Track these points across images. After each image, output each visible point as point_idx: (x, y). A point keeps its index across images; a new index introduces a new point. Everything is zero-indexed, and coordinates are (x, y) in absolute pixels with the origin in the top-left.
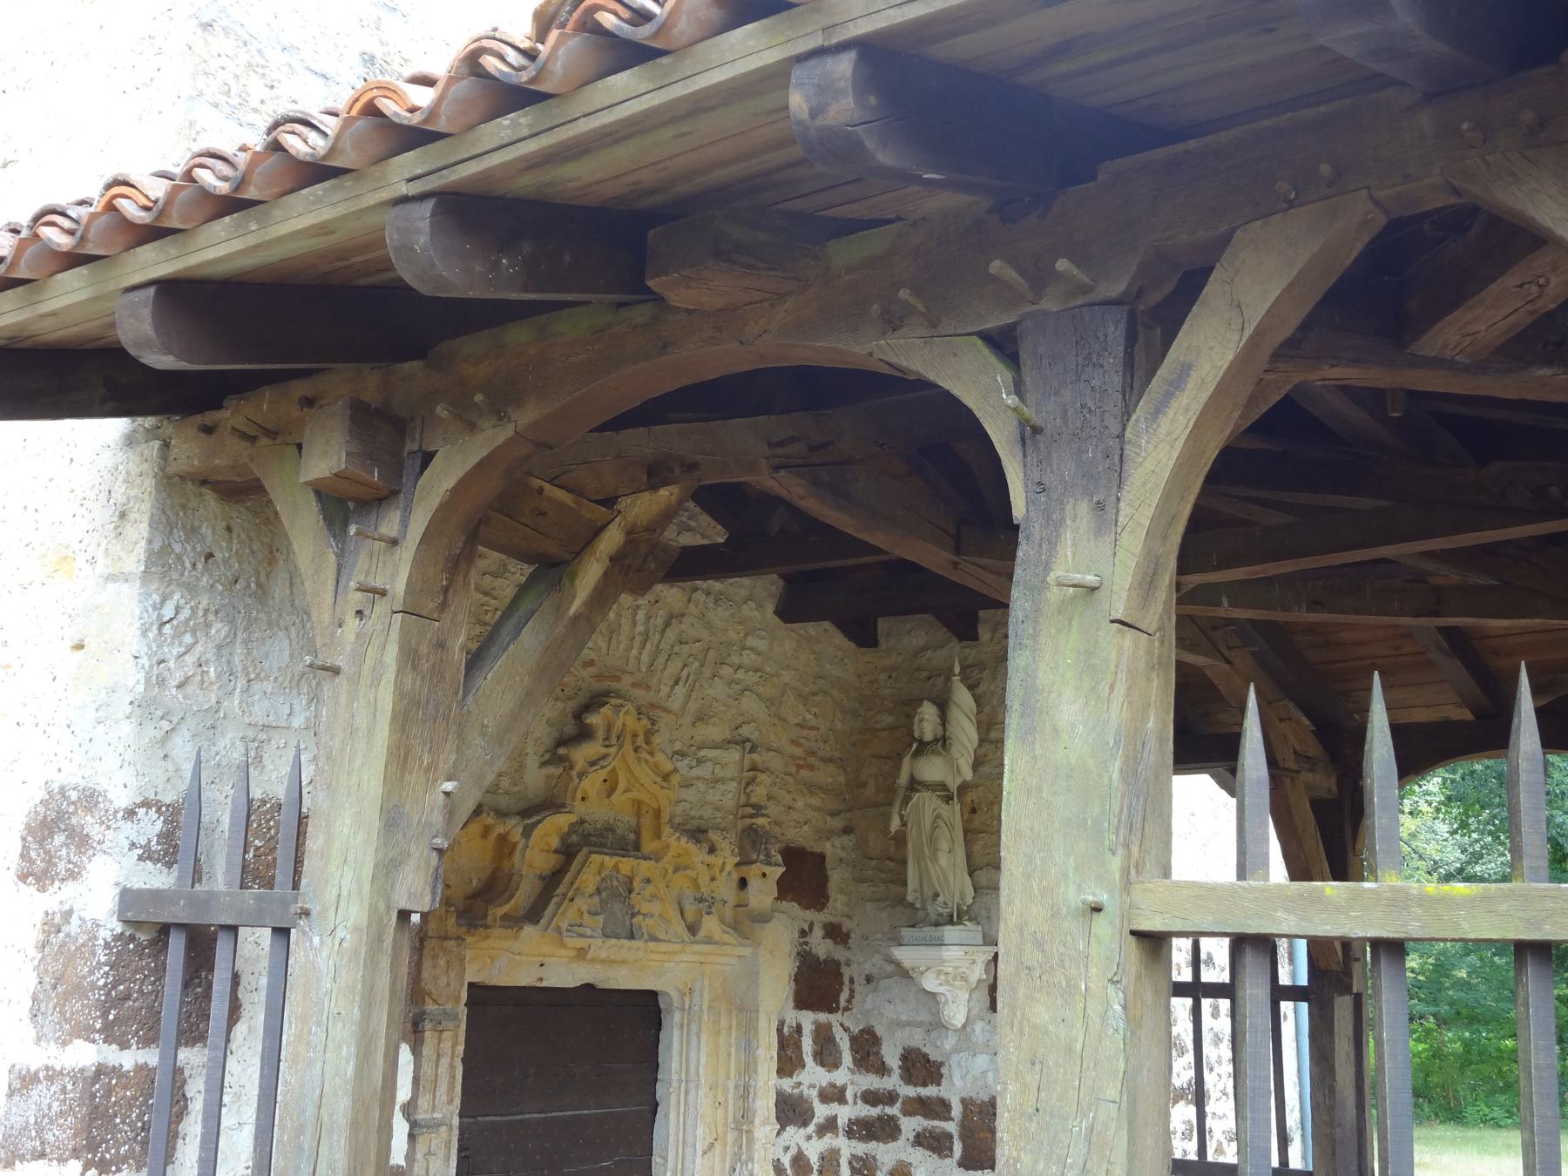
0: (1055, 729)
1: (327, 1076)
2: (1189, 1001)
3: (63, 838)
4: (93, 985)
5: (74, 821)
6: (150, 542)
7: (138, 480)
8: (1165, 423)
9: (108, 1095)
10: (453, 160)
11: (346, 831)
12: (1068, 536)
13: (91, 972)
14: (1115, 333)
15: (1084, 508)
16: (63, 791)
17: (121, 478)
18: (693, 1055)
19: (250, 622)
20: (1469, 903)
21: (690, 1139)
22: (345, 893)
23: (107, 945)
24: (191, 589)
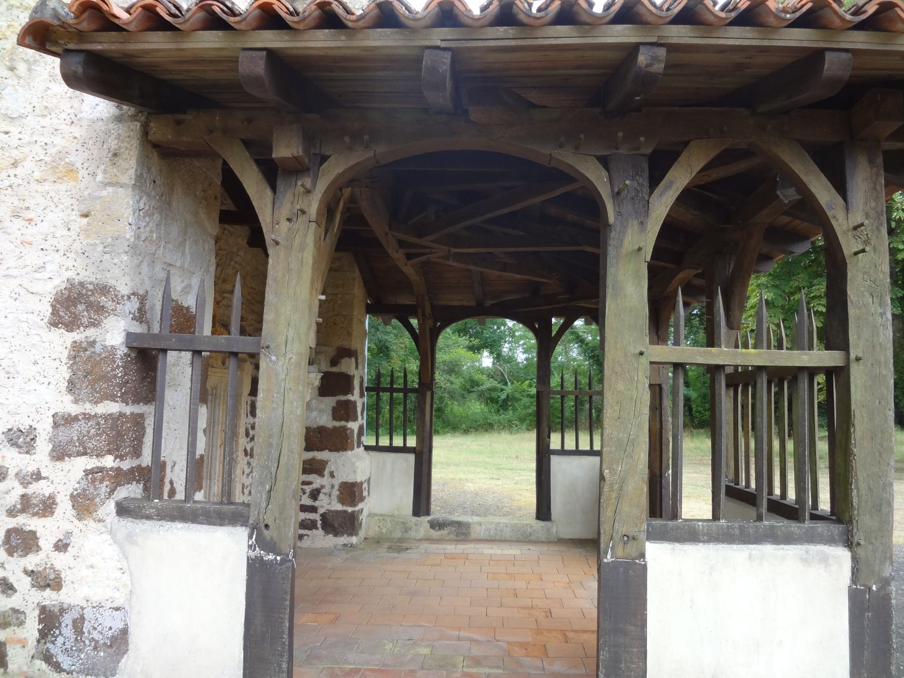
0: (625, 296)
1: (285, 414)
2: (389, 394)
3: (84, 307)
4: (115, 377)
5: (92, 299)
6: (136, 170)
7: (127, 139)
8: (664, 199)
9: (122, 427)
10: (469, 37)
11: (288, 313)
12: (629, 232)
13: (113, 370)
14: (645, 165)
15: (635, 222)
16: (81, 284)
17: (113, 137)
18: (217, 412)
19: (167, 215)
20: (755, 355)
21: (215, 444)
22: (290, 338)
23: (122, 358)
24: (148, 195)
